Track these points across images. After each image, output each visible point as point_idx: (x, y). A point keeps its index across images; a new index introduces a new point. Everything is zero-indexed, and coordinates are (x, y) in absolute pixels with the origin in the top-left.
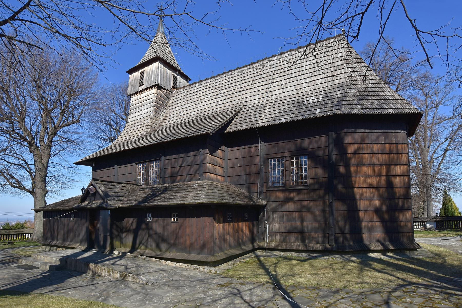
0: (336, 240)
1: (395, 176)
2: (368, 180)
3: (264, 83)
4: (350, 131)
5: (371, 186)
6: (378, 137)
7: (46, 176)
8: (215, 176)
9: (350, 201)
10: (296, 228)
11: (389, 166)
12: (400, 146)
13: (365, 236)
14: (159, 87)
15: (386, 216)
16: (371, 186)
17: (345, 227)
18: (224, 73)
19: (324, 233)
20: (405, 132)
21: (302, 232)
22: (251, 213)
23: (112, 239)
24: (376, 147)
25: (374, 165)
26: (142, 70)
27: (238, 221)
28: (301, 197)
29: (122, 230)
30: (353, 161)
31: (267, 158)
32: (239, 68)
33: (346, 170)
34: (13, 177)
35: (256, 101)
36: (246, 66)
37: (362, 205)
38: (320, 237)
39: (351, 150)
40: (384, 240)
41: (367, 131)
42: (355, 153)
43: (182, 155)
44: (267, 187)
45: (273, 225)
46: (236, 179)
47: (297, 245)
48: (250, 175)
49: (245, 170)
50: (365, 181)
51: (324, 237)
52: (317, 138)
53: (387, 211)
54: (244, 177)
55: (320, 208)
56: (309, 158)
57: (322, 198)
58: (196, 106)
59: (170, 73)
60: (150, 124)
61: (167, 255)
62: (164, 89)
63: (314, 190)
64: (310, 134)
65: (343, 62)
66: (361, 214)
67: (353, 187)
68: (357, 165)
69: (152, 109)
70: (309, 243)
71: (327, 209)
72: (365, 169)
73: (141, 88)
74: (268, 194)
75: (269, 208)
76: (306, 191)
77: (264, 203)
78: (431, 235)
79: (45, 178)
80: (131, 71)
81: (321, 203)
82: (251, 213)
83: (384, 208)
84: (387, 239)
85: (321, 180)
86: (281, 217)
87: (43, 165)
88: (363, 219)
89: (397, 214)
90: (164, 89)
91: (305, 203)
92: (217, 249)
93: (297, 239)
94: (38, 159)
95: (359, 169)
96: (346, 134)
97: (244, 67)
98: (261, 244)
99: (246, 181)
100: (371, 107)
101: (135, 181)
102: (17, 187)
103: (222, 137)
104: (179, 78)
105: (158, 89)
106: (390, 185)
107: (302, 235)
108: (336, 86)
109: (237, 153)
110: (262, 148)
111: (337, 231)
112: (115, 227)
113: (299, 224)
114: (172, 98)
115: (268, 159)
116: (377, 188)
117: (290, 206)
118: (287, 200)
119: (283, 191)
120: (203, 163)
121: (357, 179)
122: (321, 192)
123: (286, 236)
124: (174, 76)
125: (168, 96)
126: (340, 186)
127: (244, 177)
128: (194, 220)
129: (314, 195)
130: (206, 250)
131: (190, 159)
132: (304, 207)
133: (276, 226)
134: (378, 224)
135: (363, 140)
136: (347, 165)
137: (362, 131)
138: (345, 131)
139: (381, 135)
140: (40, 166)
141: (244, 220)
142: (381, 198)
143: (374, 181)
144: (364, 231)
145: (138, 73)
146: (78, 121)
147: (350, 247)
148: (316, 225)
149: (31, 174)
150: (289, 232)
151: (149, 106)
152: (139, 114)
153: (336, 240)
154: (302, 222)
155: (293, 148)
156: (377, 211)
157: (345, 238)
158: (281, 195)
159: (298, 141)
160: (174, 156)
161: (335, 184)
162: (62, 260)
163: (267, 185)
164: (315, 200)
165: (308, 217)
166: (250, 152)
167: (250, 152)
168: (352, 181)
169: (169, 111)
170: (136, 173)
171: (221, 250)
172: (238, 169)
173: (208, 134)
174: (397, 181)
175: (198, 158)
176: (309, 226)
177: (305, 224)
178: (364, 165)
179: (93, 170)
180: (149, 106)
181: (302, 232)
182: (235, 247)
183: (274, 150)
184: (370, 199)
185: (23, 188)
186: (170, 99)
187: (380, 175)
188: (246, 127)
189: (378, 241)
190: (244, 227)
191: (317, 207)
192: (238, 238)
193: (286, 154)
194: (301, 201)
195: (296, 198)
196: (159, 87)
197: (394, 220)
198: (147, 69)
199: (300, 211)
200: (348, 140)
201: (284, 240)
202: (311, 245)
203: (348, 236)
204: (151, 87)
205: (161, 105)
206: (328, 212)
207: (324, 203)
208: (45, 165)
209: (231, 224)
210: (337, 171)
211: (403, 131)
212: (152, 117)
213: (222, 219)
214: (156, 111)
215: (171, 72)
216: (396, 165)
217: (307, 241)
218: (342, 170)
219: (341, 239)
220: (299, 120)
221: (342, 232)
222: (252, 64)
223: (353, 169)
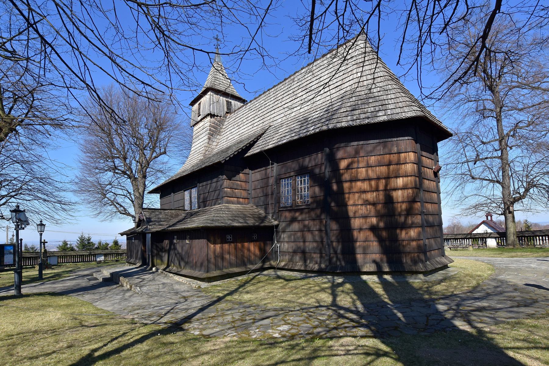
0: (330, 260)
1: (396, 189)
2: (364, 196)
3: (291, 99)
4: (342, 145)
5: (367, 203)
6: (374, 148)
7: (143, 203)
8: (236, 199)
9: (343, 220)
10: (299, 248)
11: (388, 178)
12: (402, 155)
13: (360, 257)
14: (212, 116)
15: (384, 234)
16: (367, 203)
17: (338, 247)
18: (264, 93)
19: (321, 253)
20: (410, 138)
21: (304, 252)
22: (263, 234)
23: (153, 257)
24: (373, 160)
25: (370, 180)
26: (199, 102)
27: (242, 242)
28: (304, 216)
29: (162, 250)
30: (346, 176)
31: (278, 180)
32: (275, 86)
33: (338, 187)
34: (121, 206)
35: (280, 120)
36: (281, 83)
37: (356, 223)
38: (316, 256)
39: (343, 164)
40: (382, 260)
41: (361, 143)
42: (348, 168)
43: (209, 182)
44: (279, 207)
45: (284, 244)
46: (257, 200)
47: (299, 265)
48: (269, 196)
49: (263, 191)
50: (359, 197)
51: (321, 257)
52: (314, 156)
53: (385, 228)
54: (262, 198)
55: (318, 227)
56: (310, 177)
57: (318, 218)
58: (236, 132)
59: (223, 99)
60: (204, 152)
61: (184, 272)
62: (217, 116)
63: (313, 209)
64: (309, 153)
65: (355, 66)
66: (355, 233)
67: (346, 205)
68: (351, 181)
69: (206, 137)
70: (310, 263)
71: (323, 229)
72: (359, 184)
73: (199, 118)
74: (280, 214)
75: (280, 228)
76: (306, 210)
77: (276, 223)
78: (506, 254)
79: (142, 205)
80: (193, 104)
81: (317, 222)
82: (263, 234)
83: (382, 225)
84: (385, 259)
85: (318, 199)
86: (289, 237)
87: (140, 193)
88: (357, 239)
89: (380, 232)
90: (217, 116)
91: (306, 222)
92: (212, 267)
93: (300, 258)
94: (136, 189)
95: (353, 184)
96: (338, 149)
97: (279, 84)
98: (273, 263)
99: (264, 202)
100: (361, 118)
101: (184, 206)
102: (123, 214)
103: (240, 161)
104: (233, 102)
105: (211, 118)
106: (389, 201)
107: (304, 254)
108: (348, 93)
109: (255, 176)
110: (274, 169)
111: (332, 251)
112: (155, 247)
113: (302, 244)
114: (226, 123)
115: (280, 179)
116: (374, 204)
117: (296, 226)
118: (293, 220)
119: (290, 211)
120: (221, 189)
121: (351, 196)
122: (318, 211)
123: (293, 256)
124: (227, 102)
125: (222, 122)
126: (333, 204)
127: (262, 198)
128: (197, 240)
129: (313, 214)
130: (203, 268)
131: (214, 185)
132: (305, 226)
133: (286, 246)
134: (375, 244)
135: (357, 152)
136: (340, 183)
137: (355, 143)
138: (336, 146)
139: (377, 146)
140: (137, 195)
141: (250, 241)
142: (379, 216)
143: (370, 196)
144: (359, 251)
145: (196, 105)
146: (165, 153)
147: (342, 267)
148: (315, 245)
149: (133, 202)
150: (295, 252)
151: (204, 134)
152: (198, 142)
153: (330, 260)
154: (304, 242)
155: (297, 168)
156: (373, 229)
157: (338, 258)
158: (288, 215)
159: (301, 160)
160: (205, 183)
161: (331, 203)
162: (112, 274)
163: (280, 205)
164: (313, 220)
165: (309, 237)
166: (266, 174)
167: (266, 174)
168: (344, 199)
169: (222, 137)
170: (184, 199)
171: (217, 267)
172: (258, 191)
173: (219, 163)
174: (398, 195)
175: (219, 183)
176: (310, 246)
177: (307, 244)
178: (359, 180)
179: (161, 197)
180: (204, 134)
181: (304, 252)
182: (237, 266)
183: (283, 171)
184: (365, 217)
185: (129, 214)
186: (223, 125)
187: (377, 190)
188: (258, 151)
189: (374, 261)
190: (253, 248)
191: (314, 226)
192: (243, 256)
193: (292, 174)
194: (303, 220)
195: (300, 218)
196: (212, 116)
197: (394, 239)
198: (203, 100)
199: (302, 231)
200: (340, 154)
201: (291, 260)
202: (311, 265)
203: (340, 256)
204: (205, 117)
205: (214, 132)
206: (324, 231)
207: (321, 222)
208: (142, 193)
209: (233, 244)
210: (331, 187)
211: (406, 138)
212: (206, 145)
213: (219, 241)
214: (209, 139)
215: (224, 98)
216: (397, 177)
217: (308, 261)
218: (335, 187)
219: (334, 259)
220: (295, 140)
221: (336, 253)
222: (285, 80)
223: (346, 185)
